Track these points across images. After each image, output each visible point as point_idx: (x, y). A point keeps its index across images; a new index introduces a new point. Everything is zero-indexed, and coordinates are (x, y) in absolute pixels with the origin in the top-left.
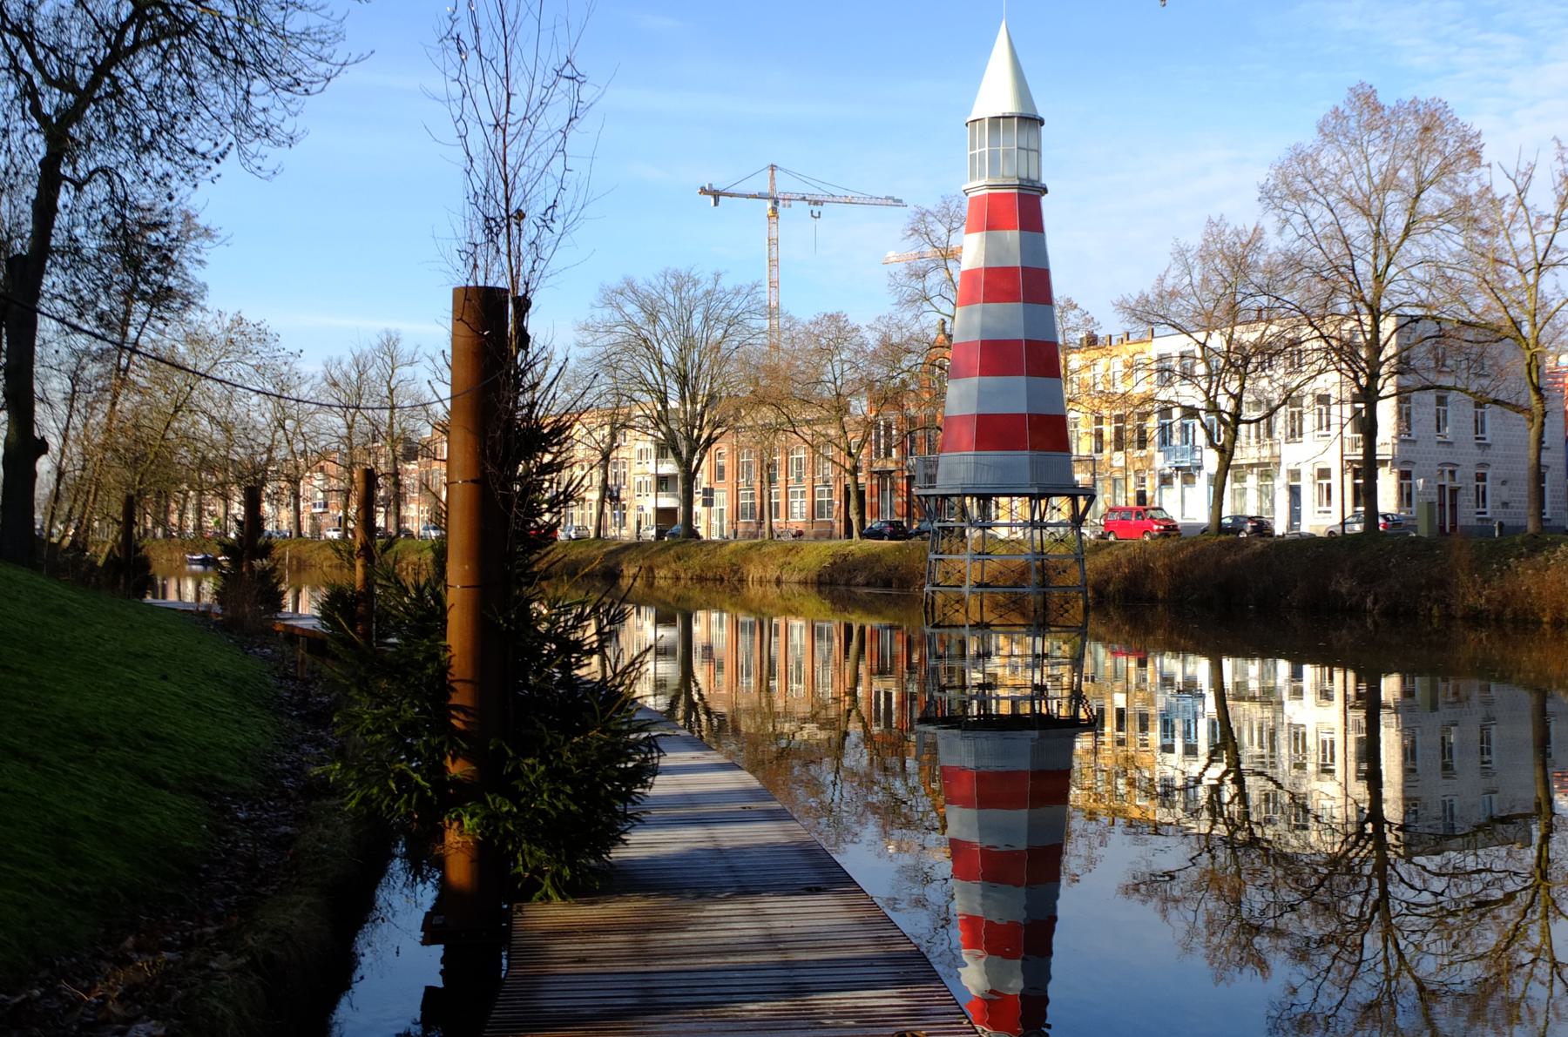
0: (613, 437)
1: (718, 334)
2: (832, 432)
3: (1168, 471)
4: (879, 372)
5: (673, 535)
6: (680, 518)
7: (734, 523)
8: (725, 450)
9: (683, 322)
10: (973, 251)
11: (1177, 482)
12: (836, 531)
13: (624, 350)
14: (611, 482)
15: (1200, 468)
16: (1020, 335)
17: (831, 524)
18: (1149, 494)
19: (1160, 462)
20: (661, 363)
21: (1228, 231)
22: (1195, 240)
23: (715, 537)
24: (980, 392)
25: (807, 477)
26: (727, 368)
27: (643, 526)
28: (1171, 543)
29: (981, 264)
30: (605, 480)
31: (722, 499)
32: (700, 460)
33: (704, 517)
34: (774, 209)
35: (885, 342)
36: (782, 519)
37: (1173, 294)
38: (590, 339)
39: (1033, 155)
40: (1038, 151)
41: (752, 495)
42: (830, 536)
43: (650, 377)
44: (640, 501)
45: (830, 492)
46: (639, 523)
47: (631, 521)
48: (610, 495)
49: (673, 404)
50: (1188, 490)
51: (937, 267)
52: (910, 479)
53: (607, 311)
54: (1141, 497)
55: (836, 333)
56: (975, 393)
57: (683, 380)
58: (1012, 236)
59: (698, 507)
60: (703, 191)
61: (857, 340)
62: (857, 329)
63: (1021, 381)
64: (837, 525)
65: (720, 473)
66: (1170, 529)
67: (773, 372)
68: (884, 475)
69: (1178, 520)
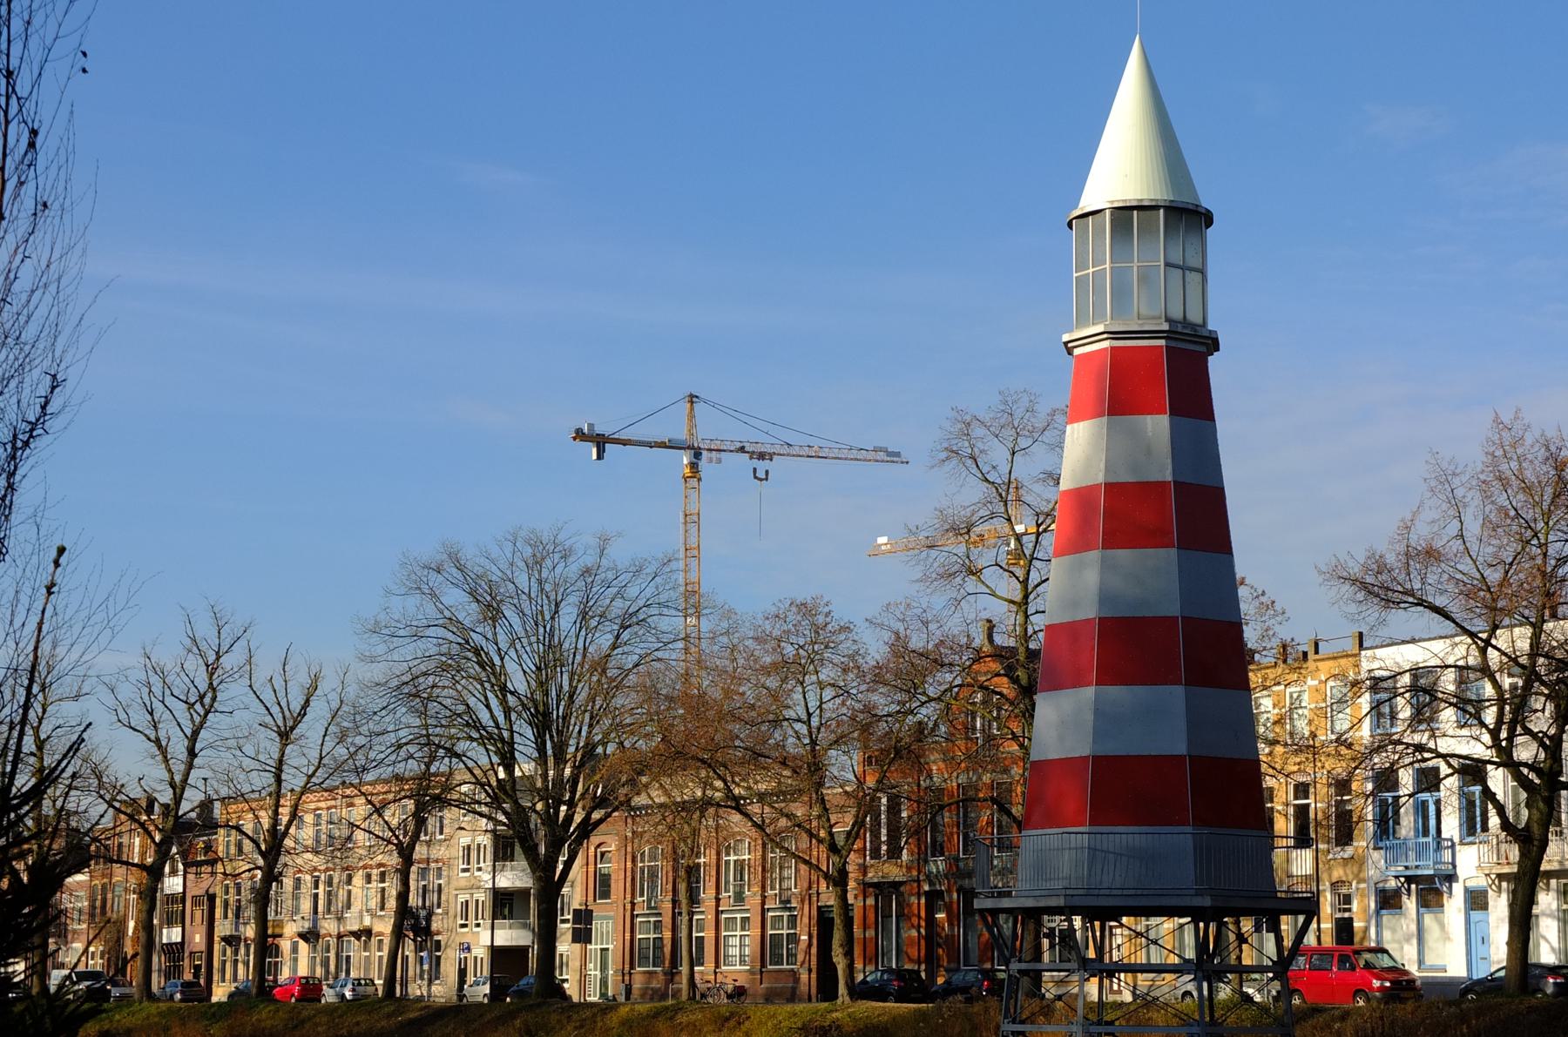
0: (420, 823)
1: (604, 640)
2: (799, 811)
3: (1392, 884)
4: (884, 702)
5: (521, 994)
6: (533, 963)
7: (626, 974)
8: (612, 847)
9: (544, 624)
10: (1081, 452)
11: (1410, 904)
12: (803, 988)
13: (444, 668)
14: (414, 900)
15: (1451, 878)
16: (1171, 607)
17: (794, 975)
18: (1357, 924)
19: (1379, 867)
20: (504, 689)
21: (1529, 439)
22: (1471, 455)
23: (594, 998)
24: (1098, 712)
25: (752, 896)
26: (619, 701)
27: (470, 979)
28: (1404, 1010)
29: (1100, 478)
30: (403, 897)
31: (608, 931)
32: (568, 865)
33: (575, 964)
34: (694, 466)
35: (899, 647)
36: (709, 965)
37: (1431, 555)
38: (381, 649)
39: (1193, 278)
40: (1202, 272)
41: (658, 926)
42: (793, 997)
43: (484, 716)
44: (465, 935)
45: (793, 921)
46: (462, 973)
47: (449, 970)
48: (413, 924)
49: (525, 767)
50: (1428, 919)
51: (992, 516)
52: (933, 898)
53: (413, 601)
54: (1344, 928)
55: (808, 641)
56: (1089, 717)
57: (542, 722)
58: (1157, 426)
59: (565, 946)
60: (580, 435)
61: (847, 647)
62: (845, 629)
63: (1175, 695)
64: (804, 977)
65: (603, 886)
66: (1402, 985)
67: (697, 705)
68: (884, 890)
69: (1413, 969)
